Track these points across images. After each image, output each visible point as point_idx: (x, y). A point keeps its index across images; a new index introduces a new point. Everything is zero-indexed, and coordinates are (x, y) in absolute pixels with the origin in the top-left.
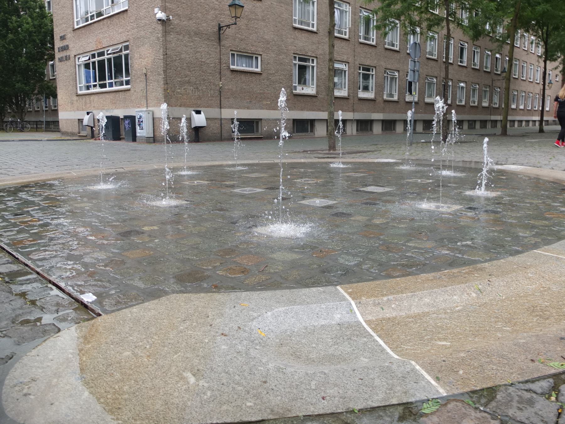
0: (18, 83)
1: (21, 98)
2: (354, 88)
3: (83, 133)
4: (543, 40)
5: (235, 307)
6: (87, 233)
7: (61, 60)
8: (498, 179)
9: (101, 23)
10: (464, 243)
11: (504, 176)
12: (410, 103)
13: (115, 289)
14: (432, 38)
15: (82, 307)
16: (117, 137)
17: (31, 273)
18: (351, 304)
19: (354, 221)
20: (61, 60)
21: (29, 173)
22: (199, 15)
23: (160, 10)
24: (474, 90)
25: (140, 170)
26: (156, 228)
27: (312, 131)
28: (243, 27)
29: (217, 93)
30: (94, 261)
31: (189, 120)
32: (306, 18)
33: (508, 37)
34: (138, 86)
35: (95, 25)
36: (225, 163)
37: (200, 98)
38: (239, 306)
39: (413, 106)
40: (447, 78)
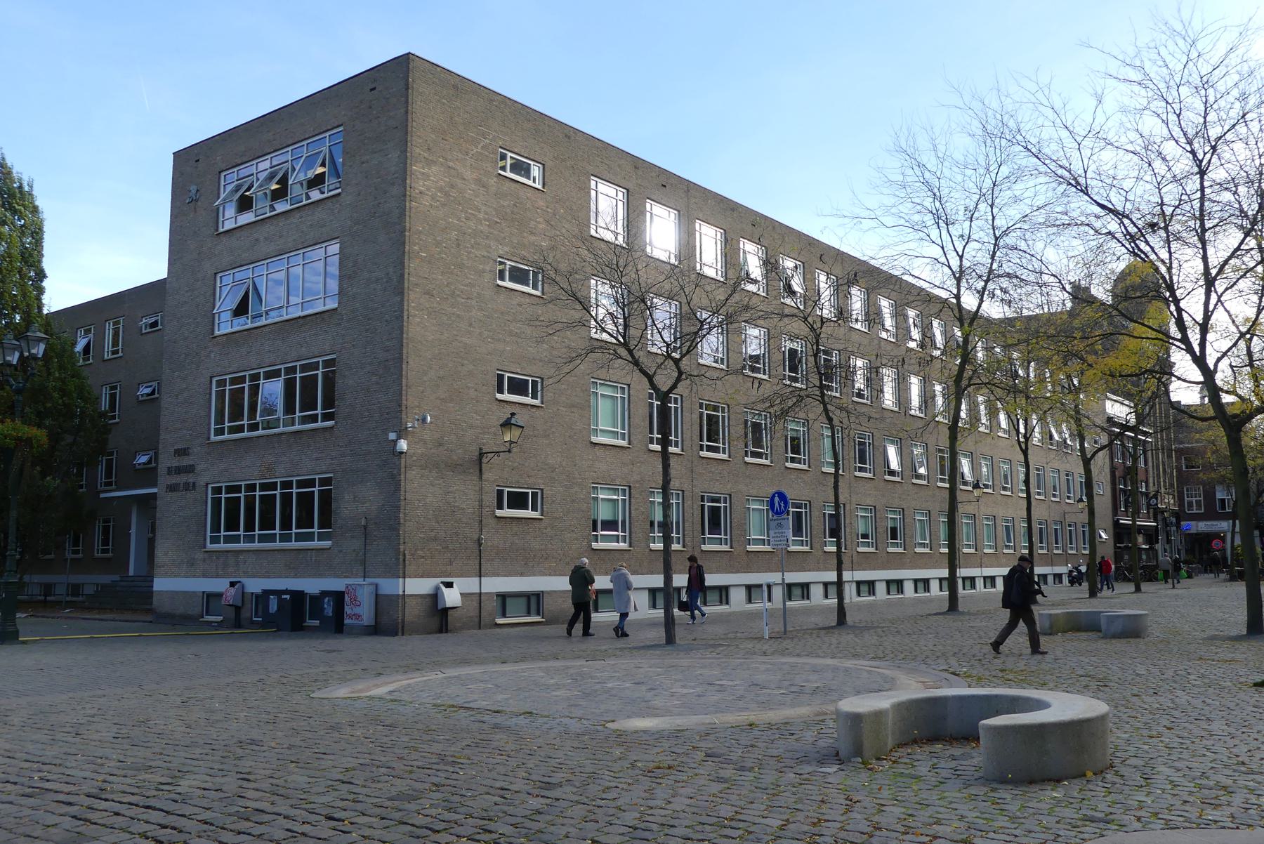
7: (172, 488)
20: (172, 488)
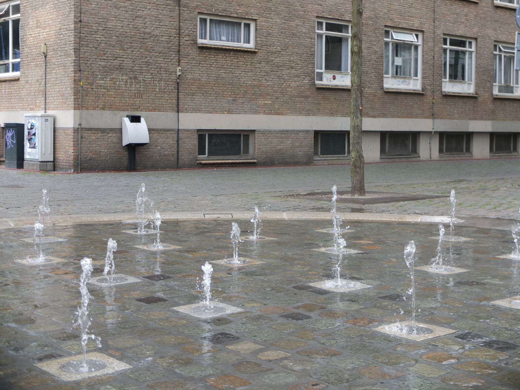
2: (433, 77)
29: (172, 87)
34: (32, 74)
37: (139, 94)
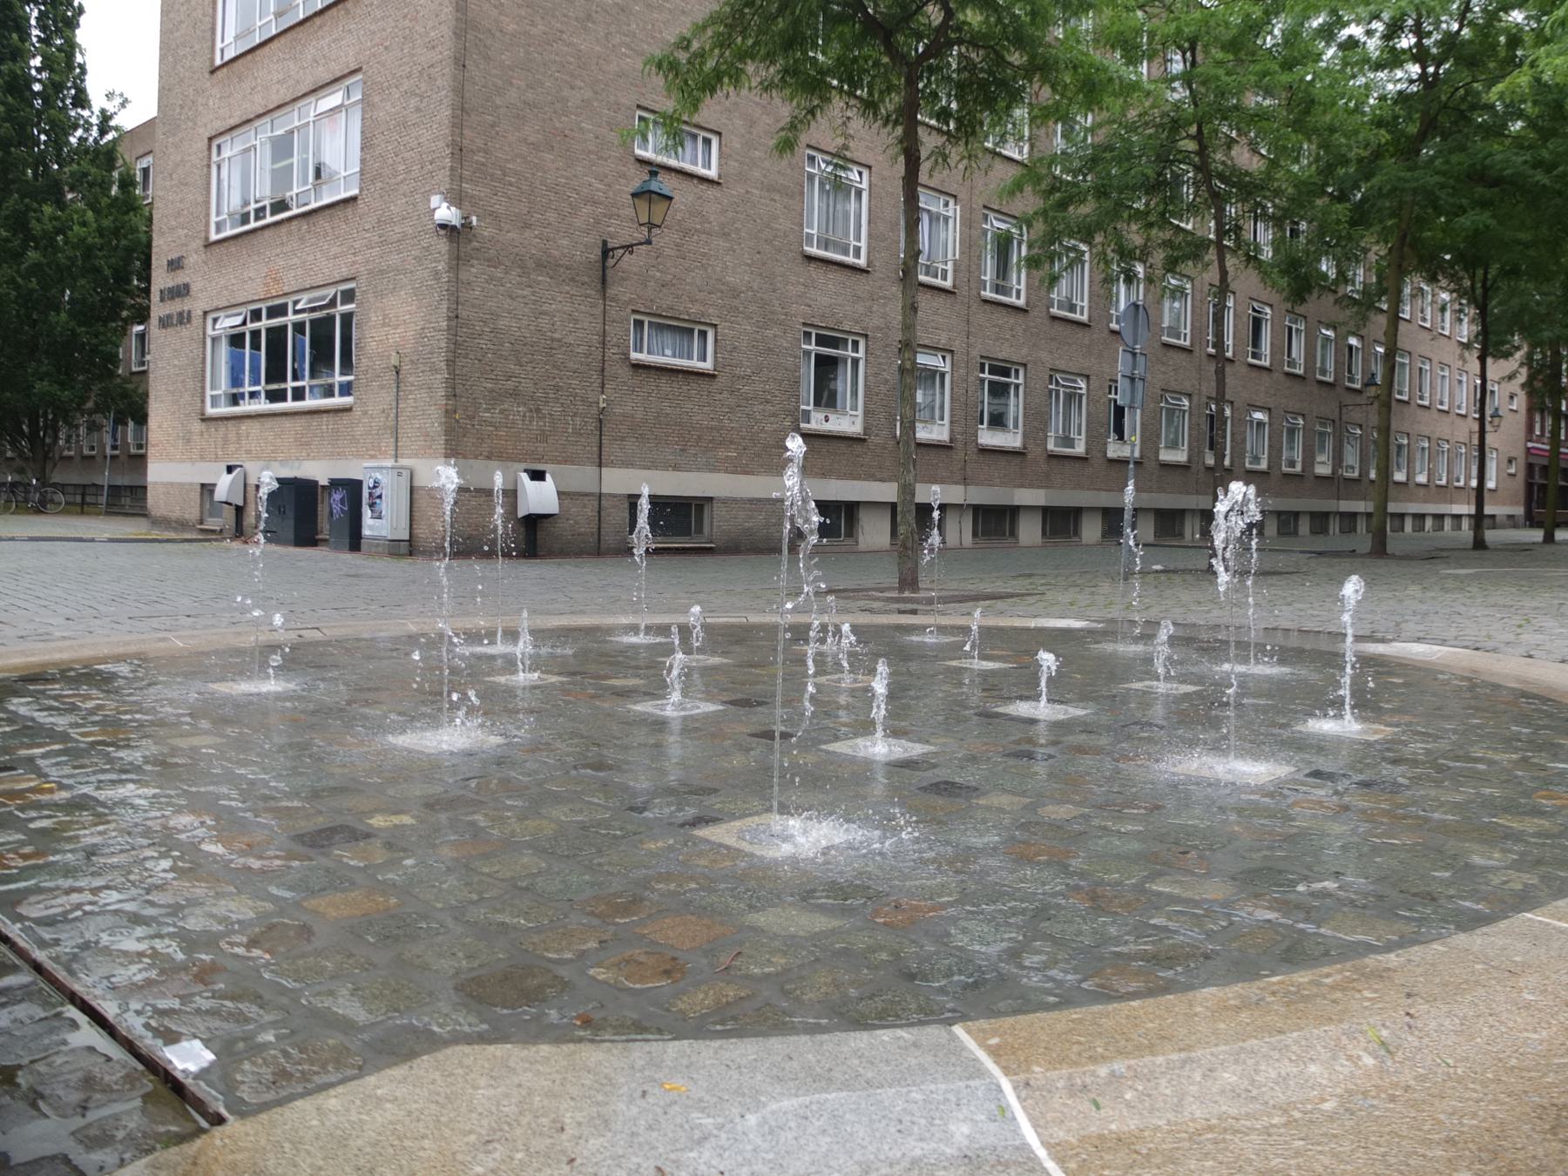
0: (41, 379)
1: (46, 420)
2: (966, 419)
3: (213, 523)
4: (1473, 300)
5: (644, 1094)
6: (201, 832)
7: (165, 323)
8: (1383, 688)
9: (284, 229)
10: (1318, 886)
11: (1398, 676)
12: (1123, 462)
13: (274, 1024)
14: (1178, 293)
15: (164, 1091)
16: (306, 536)
17: (14, 969)
18: (999, 1089)
19: (988, 808)
20: (165, 323)
21: (45, 637)
22: (552, 216)
23: (445, 199)
24: (1291, 432)
25: (365, 635)
26: (407, 820)
27: (851, 533)
28: (667, 251)
29: (592, 426)
30: (217, 928)
31: (511, 494)
32: (840, 232)
33: (1382, 292)
34: (374, 401)
35: (267, 233)
36: (608, 620)
37: (543, 436)
38: (656, 1091)
39: (1131, 474)
40: (1220, 398)
